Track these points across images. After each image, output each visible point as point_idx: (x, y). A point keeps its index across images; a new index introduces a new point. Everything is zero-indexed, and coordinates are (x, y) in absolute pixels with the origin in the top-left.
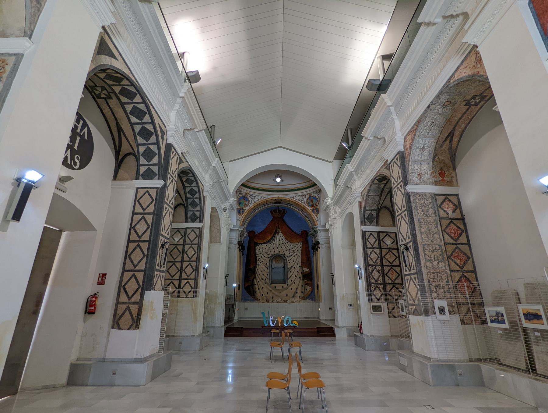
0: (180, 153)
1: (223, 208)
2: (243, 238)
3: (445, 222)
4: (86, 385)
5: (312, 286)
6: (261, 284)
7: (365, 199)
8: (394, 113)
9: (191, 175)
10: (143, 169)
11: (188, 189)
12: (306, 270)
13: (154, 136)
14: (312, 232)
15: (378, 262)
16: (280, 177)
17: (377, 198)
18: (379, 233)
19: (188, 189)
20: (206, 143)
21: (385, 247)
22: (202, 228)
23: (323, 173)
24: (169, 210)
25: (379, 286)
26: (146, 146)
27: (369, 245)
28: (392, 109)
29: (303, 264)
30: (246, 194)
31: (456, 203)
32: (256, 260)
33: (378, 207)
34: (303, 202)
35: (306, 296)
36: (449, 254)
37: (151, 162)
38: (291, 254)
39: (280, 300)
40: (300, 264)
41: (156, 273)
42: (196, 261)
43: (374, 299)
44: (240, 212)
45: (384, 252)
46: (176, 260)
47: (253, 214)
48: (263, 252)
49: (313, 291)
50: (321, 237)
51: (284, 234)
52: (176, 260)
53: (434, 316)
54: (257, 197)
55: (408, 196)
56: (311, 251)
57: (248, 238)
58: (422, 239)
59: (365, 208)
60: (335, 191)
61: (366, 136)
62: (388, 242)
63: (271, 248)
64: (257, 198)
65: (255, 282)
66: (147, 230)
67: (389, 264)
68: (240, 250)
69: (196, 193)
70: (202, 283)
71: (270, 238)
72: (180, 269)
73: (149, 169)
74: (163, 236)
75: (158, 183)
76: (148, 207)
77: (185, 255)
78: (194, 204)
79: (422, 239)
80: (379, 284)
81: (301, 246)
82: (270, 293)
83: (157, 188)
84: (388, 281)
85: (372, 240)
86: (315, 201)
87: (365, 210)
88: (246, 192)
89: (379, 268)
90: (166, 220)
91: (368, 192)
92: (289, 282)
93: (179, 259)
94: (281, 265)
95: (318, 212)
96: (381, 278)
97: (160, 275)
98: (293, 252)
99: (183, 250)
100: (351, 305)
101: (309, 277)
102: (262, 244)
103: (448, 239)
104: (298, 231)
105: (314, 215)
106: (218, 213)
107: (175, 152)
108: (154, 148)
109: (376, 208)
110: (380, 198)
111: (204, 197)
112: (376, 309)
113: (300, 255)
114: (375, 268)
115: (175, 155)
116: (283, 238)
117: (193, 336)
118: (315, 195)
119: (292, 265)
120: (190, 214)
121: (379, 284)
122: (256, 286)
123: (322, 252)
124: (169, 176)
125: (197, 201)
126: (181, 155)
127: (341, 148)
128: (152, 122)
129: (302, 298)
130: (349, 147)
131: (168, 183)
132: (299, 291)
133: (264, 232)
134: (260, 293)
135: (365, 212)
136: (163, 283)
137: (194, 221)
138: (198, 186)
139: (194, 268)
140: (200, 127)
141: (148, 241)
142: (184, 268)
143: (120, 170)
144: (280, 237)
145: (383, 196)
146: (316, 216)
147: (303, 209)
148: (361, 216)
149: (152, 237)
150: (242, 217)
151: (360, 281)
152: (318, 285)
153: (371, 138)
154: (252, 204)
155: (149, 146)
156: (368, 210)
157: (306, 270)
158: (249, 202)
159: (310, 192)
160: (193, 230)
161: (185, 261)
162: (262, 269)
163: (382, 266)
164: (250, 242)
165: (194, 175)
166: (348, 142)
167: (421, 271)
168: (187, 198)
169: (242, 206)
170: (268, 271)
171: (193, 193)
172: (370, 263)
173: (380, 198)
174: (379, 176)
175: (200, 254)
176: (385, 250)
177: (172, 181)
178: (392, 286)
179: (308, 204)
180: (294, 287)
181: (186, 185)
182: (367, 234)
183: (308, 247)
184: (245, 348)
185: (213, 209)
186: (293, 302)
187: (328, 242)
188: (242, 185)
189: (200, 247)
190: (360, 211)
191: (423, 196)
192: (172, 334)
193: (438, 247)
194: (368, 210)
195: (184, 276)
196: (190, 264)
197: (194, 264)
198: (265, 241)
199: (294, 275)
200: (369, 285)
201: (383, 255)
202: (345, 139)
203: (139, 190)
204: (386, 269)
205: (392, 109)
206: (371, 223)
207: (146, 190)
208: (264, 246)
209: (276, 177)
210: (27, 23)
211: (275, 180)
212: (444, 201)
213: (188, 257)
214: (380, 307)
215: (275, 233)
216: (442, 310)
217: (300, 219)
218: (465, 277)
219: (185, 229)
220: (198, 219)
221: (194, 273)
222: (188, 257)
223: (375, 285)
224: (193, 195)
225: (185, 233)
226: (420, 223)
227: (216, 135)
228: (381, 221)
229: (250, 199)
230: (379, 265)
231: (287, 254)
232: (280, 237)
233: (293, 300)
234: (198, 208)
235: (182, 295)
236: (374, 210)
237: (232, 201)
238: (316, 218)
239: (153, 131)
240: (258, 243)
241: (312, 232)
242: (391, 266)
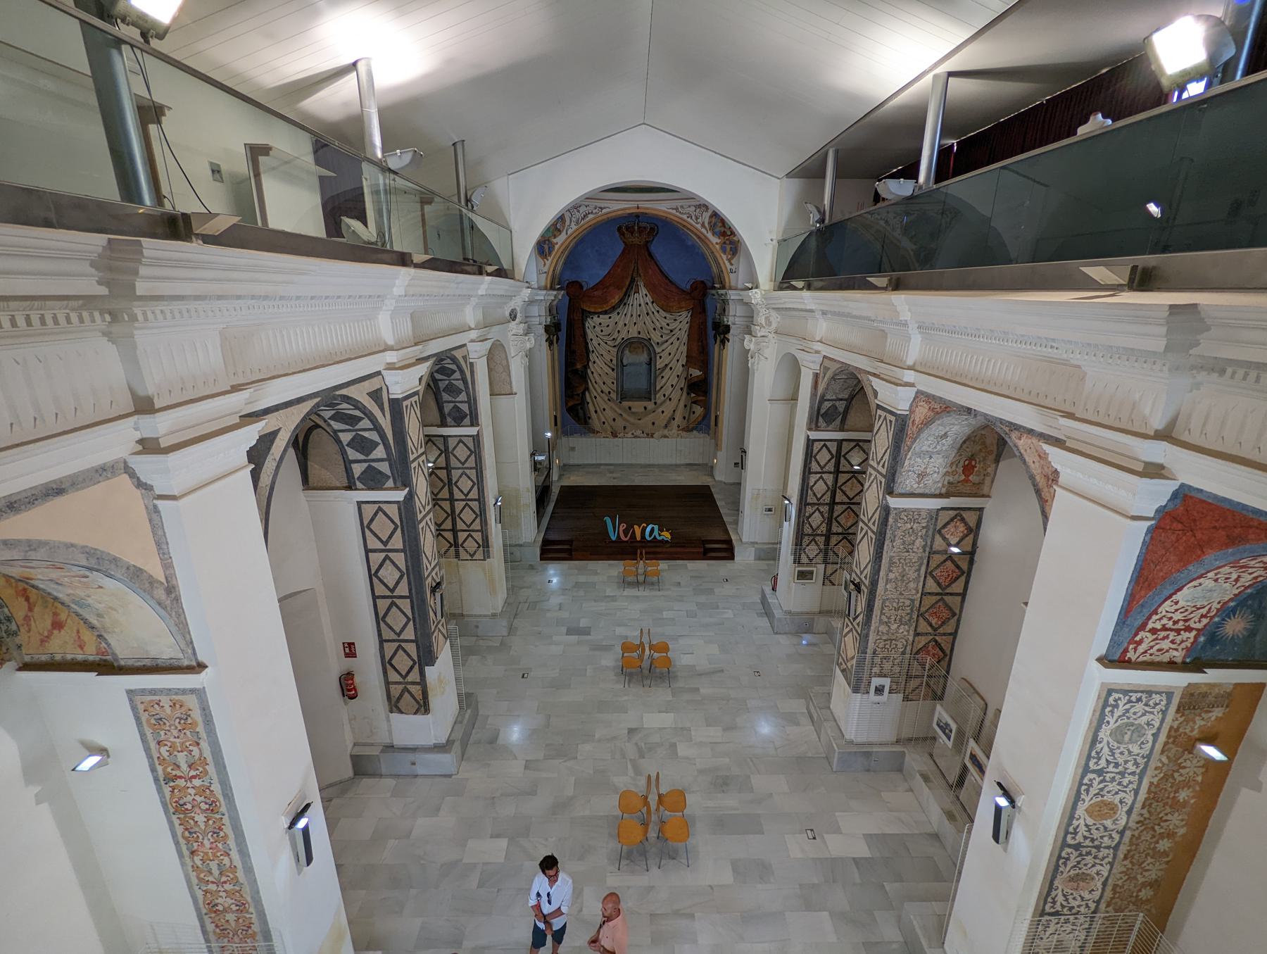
3: (938, 559)
4: (381, 776)
6: (601, 402)
10: (358, 469)
12: (696, 373)
29: (690, 361)
31: (972, 524)
36: (923, 609)
38: (665, 338)
39: (639, 432)
40: (683, 360)
42: (478, 500)
43: (804, 559)
45: (843, 478)
48: (603, 331)
49: (706, 415)
51: (651, 288)
53: (865, 696)
55: (886, 510)
58: (886, 590)
63: (621, 324)
65: (588, 399)
70: (495, 530)
78: (451, 389)
79: (886, 590)
81: (688, 319)
82: (619, 420)
83: (398, 502)
85: (824, 457)
87: (823, 400)
94: (644, 358)
98: (670, 332)
99: (450, 480)
100: (770, 510)
101: (701, 389)
102: (599, 314)
103: (931, 586)
104: (684, 282)
112: (803, 575)
113: (685, 339)
116: (649, 299)
117: (494, 615)
120: (448, 408)
122: (590, 405)
129: (683, 430)
132: (678, 416)
134: (599, 419)
135: (821, 403)
137: (458, 424)
143: (309, 463)
144: (642, 297)
146: (729, 260)
148: (811, 407)
151: (786, 524)
152: (716, 417)
157: (696, 373)
160: (461, 441)
162: (600, 369)
167: (867, 636)
180: (668, 408)
186: (666, 437)
190: (814, 394)
191: (913, 515)
192: (457, 611)
193: (908, 603)
200: (799, 536)
203: (363, 506)
208: (604, 319)
210: (179, 637)
212: (952, 520)
214: (812, 572)
216: (879, 690)
218: (936, 641)
219: (445, 438)
226: (891, 563)
231: (656, 337)
232: (642, 297)
233: (666, 432)
234: (463, 397)
235: (463, 554)
238: (729, 266)
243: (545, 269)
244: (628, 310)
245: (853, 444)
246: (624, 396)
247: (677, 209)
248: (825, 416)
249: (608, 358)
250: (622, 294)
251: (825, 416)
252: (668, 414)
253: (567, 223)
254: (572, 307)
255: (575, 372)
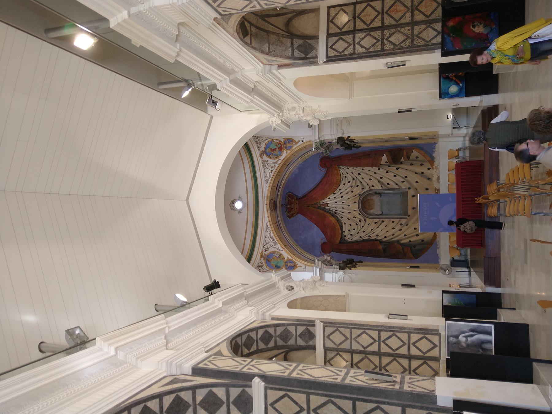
0: (205, 355)
1: (287, 292)
2: (333, 262)
5: (410, 149)
6: (409, 231)
7: (274, 59)
8: (141, 8)
9: (239, 340)
11: (262, 346)
12: (384, 158)
13: (182, 394)
14: (322, 150)
15: (377, 34)
16: (234, 202)
17: (273, 38)
18: (329, 35)
19: (262, 346)
20: (186, 315)
21: (351, 24)
22: (324, 322)
23: (234, 125)
24: (301, 370)
25: (416, 32)
26: (198, 407)
27: (349, 51)
28: (134, 10)
29: (376, 164)
30: (262, 256)
32: (370, 241)
33: (288, 37)
34: (274, 164)
35: (429, 159)
37: (224, 399)
38: (358, 184)
40: (375, 169)
41: (406, 388)
44: (291, 266)
45: (360, 25)
46: (378, 364)
47: (294, 246)
48: (355, 229)
49: (419, 147)
50: (331, 135)
51: (325, 194)
52: (378, 364)
54: (268, 240)
56: (354, 150)
57: (333, 254)
59: (289, 58)
60: (260, 110)
61: (174, 54)
62: (344, 19)
64: (269, 239)
66: (335, 404)
67: (380, 17)
68: (354, 267)
69: (266, 332)
70: (415, 321)
71: (332, 219)
72: (392, 358)
73: (235, 403)
74: (344, 379)
75: (258, 388)
76: (296, 403)
77: (368, 349)
78: (285, 336)
80: (413, 32)
81: (345, 168)
83: (266, 389)
84: (407, 18)
85: (341, 46)
86: (274, 146)
87: (293, 57)
88: (259, 256)
89: (387, 33)
90: (318, 372)
91: (263, 52)
92: (405, 185)
93: (375, 359)
94: (376, 199)
95: (290, 141)
96: (402, 30)
97: (410, 383)
99: (360, 352)
101: (396, 153)
102: (342, 231)
104: (320, 173)
105: (295, 147)
106: (296, 300)
107: (206, 362)
108: (201, 395)
109: (289, 40)
110: (274, 33)
111: (273, 319)
113: (359, 169)
114: (387, 39)
115: (210, 361)
116: (332, 196)
118: (263, 145)
119: (376, 181)
120: (301, 342)
121: (413, 32)
122: (412, 239)
123: (355, 133)
124: (245, 370)
125: (279, 330)
126: (210, 353)
127: (192, 101)
128: (160, 396)
130: (189, 86)
131: (256, 371)
132: (420, 169)
133: (323, 228)
136: (421, 378)
137: (312, 336)
138: (256, 329)
139: (390, 334)
140: (162, 324)
141: (354, 400)
142: (390, 351)
144: (332, 202)
145: (270, 28)
146: (297, 143)
147: (286, 164)
149: (348, 395)
150: (299, 262)
152: (410, 139)
153: (178, 47)
154: (278, 247)
155: (198, 401)
156: (293, 53)
157: (384, 158)
158: (274, 252)
159: (258, 153)
161: (379, 349)
162: (383, 231)
163: (383, 28)
164: (339, 251)
165: (240, 335)
166: (181, 90)
168: (276, 347)
169: (282, 264)
170: (386, 221)
171: (267, 338)
172: (378, 47)
173: (274, 33)
174: (238, 33)
175: (367, 325)
176: (357, 23)
177: (253, 366)
178: (416, 12)
179: (277, 156)
180: (413, 178)
181: (254, 348)
182: (332, 53)
183: (347, 156)
184: (522, 248)
185: (292, 305)
186: (438, 179)
187: (338, 122)
188: (249, 260)
189: (356, 325)
194: (293, 53)
195: (404, 351)
196: (384, 342)
197: (384, 335)
198: (338, 226)
199: (394, 179)
201: (365, 27)
202: (175, 94)
204: (388, 21)
205: (134, 10)
206: (312, 48)
207: (269, 408)
208: (346, 228)
209: (233, 208)
211: (240, 211)
213: (371, 344)
215: (325, 210)
217: (301, 169)
219: (326, 350)
220: (310, 328)
221: (398, 334)
222: (371, 344)
223: (416, 38)
224: (271, 336)
225: (332, 350)
227: (171, 303)
228: (309, 31)
229: (271, 250)
230: (382, 33)
231: (358, 191)
232: (332, 202)
233: (434, 179)
234: (292, 329)
236: (292, 43)
237: (274, 276)
238: (300, 143)
239: (173, 396)
240: (341, 238)
241: (322, 150)
242: (383, 14)
243: (303, 266)
244: (339, 210)
245: (331, 25)
246: (405, 214)
247: (267, 180)
248: (306, 53)
249: (373, 226)
250: (329, 215)
251: (306, 53)
252: (418, 178)
253: (276, 250)
254: (338, 250)
255: (385, 250)
